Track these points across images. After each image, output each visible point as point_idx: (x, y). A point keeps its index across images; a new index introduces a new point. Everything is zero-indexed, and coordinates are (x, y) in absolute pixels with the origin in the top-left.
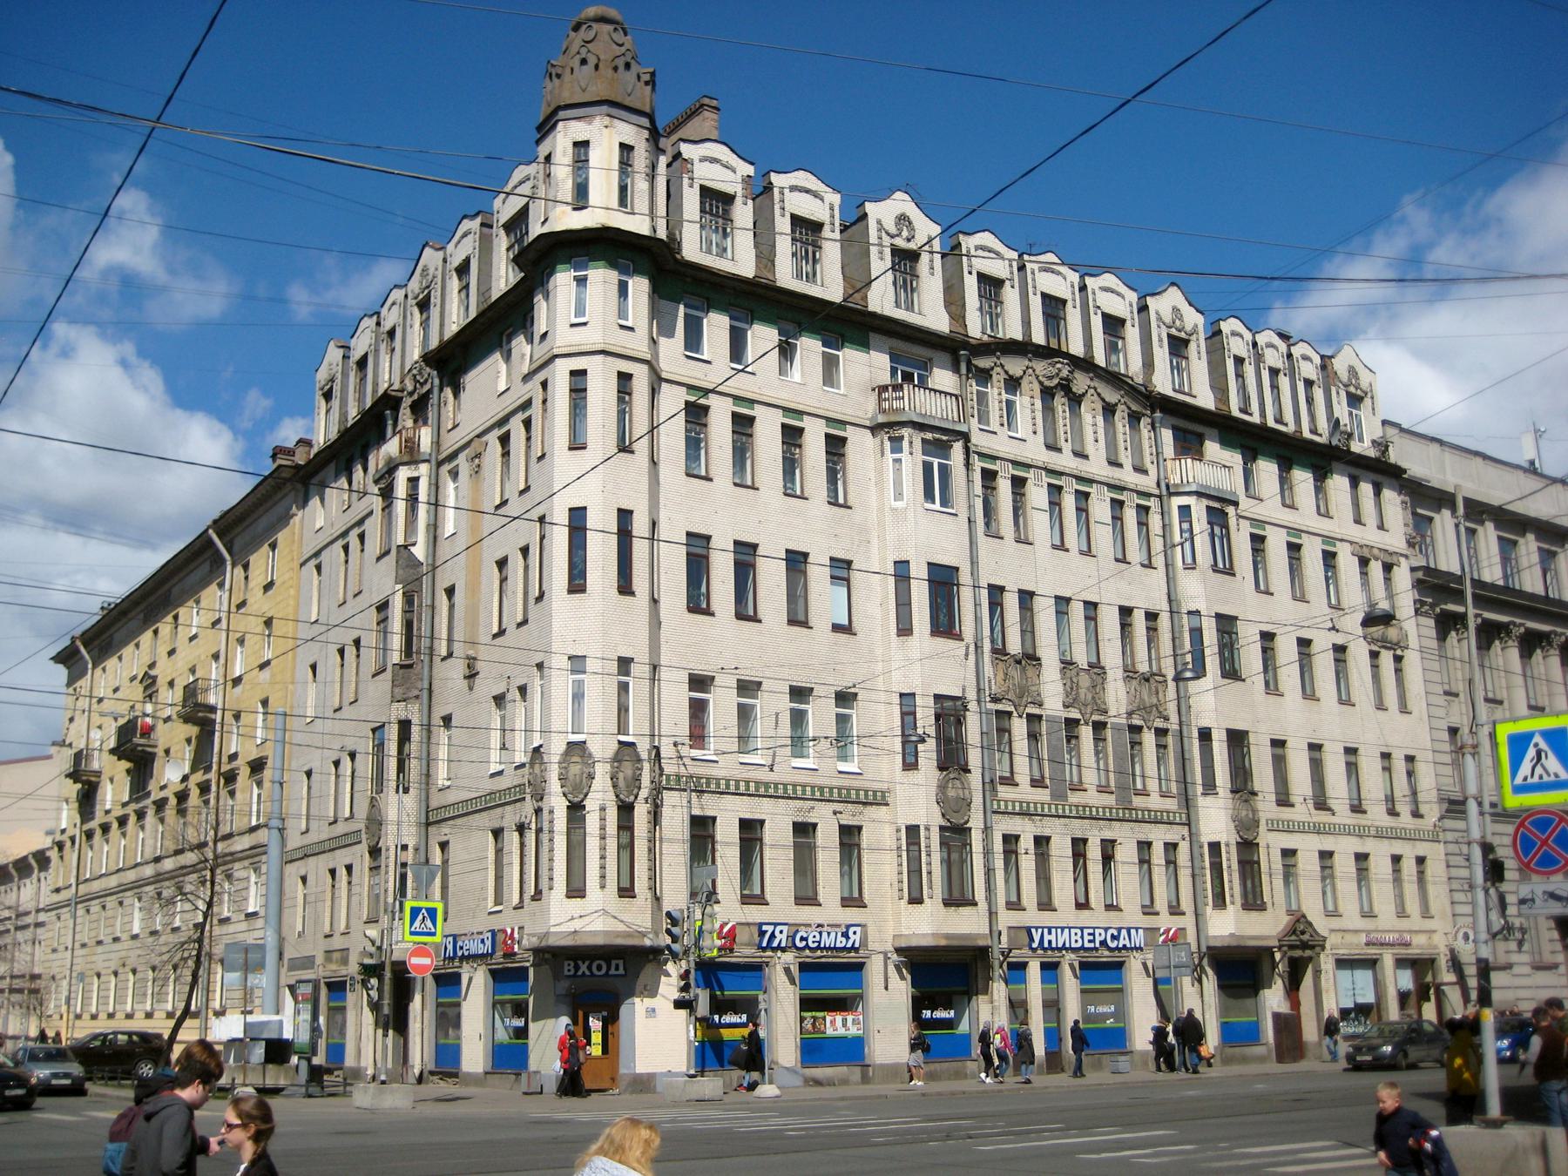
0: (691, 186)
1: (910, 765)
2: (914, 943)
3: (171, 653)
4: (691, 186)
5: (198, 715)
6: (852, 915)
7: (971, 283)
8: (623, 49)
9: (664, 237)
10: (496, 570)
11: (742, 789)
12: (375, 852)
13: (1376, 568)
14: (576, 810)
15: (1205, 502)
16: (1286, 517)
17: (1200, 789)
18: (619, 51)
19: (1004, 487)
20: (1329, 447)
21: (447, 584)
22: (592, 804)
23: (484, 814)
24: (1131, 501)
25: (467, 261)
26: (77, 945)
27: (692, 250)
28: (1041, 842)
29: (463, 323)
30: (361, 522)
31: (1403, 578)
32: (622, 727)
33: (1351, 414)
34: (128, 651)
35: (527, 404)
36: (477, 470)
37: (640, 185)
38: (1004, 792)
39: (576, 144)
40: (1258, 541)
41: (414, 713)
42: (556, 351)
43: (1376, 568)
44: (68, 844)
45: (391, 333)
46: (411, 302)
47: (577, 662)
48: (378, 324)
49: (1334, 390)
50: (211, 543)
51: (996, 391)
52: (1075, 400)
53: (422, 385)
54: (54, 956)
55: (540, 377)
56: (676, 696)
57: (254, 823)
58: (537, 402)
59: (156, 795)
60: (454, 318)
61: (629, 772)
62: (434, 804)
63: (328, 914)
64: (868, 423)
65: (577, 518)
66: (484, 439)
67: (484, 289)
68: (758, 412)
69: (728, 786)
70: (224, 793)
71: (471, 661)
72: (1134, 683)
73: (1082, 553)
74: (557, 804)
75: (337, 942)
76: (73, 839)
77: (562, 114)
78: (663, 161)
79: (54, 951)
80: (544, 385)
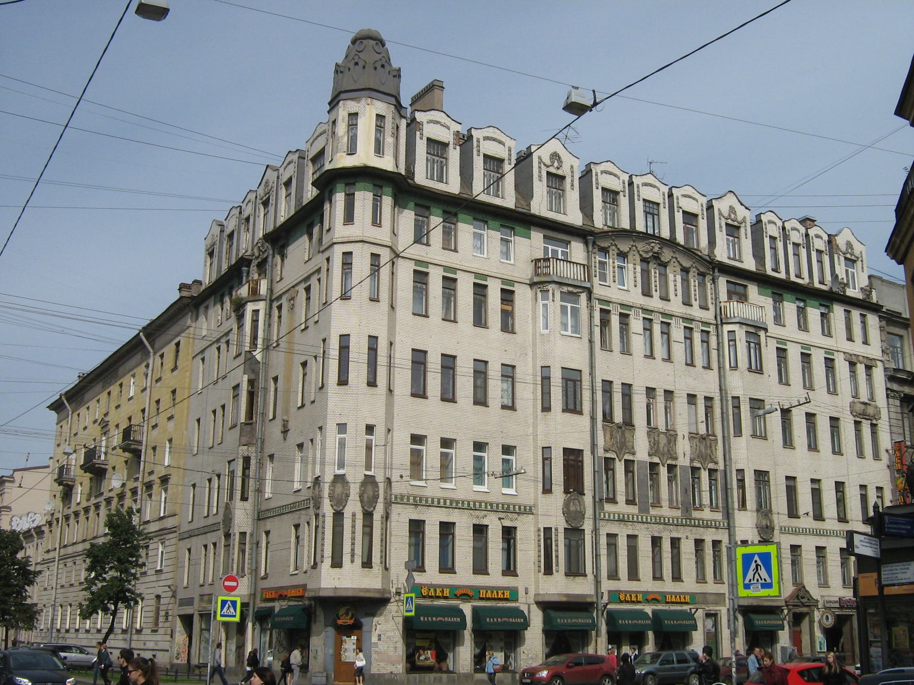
0: (421, 139)
2: (547, 599)
3: (118, 407)
5: (131, 447)
6: (508, 581)
7: (597, 195)
8: (381, 56)
11: (442, 504)
12: (228, 536)
13: (861, 369)
14: (338, 516)
15: (745, 328)
16: (802, 337)
17: (736, 506)
18: (378, 57)
19: (615, 320)
20: (831, 291)
22: (347, 513)
23: (290, 515)
24: (697, 328)
25: (290, 180)
26: (59, 586)
27: (421, 178)
28: (632, 538)
29: (287, 217)
30: (227, 334)
31: (879, 374)
32: (368, 467)
33: (847, 271)
34: (92, 404)
35: (318, 271)
36: (292, 308)
37: (389, 140)
38: (608, 507)
39: (350, 115)
40: (782, 353)
41: (252, 452)
42: (335, 240)
43: (861, 369)
44: (55, 522)
45: (248, 219)
46: (259, 201)
47: (342, 428)
48: (240, 213)
49: (836, 256)
50: (141, 342)
51: (611, 261)
52: (664, 265)
53: (263, 253)
54: (45, 593)
56: (402, 448)
57: (162, 515)
58: (324, 270)
59: (107, 495)
60: (283, 214)
61: (371, 494)
62: (263, 508)
63: (202, 570)
64: (528, 282)
66: (297, 288)
67: (299, 198)
70: (145, 496)
71: (285, 424)
72: (695, 440)
73: (663, 360)
74: (327, 509)
75: (207, 590)
77: (343, 96)
78: (403, 123)
79: (45, 589)
80: (328, 259)
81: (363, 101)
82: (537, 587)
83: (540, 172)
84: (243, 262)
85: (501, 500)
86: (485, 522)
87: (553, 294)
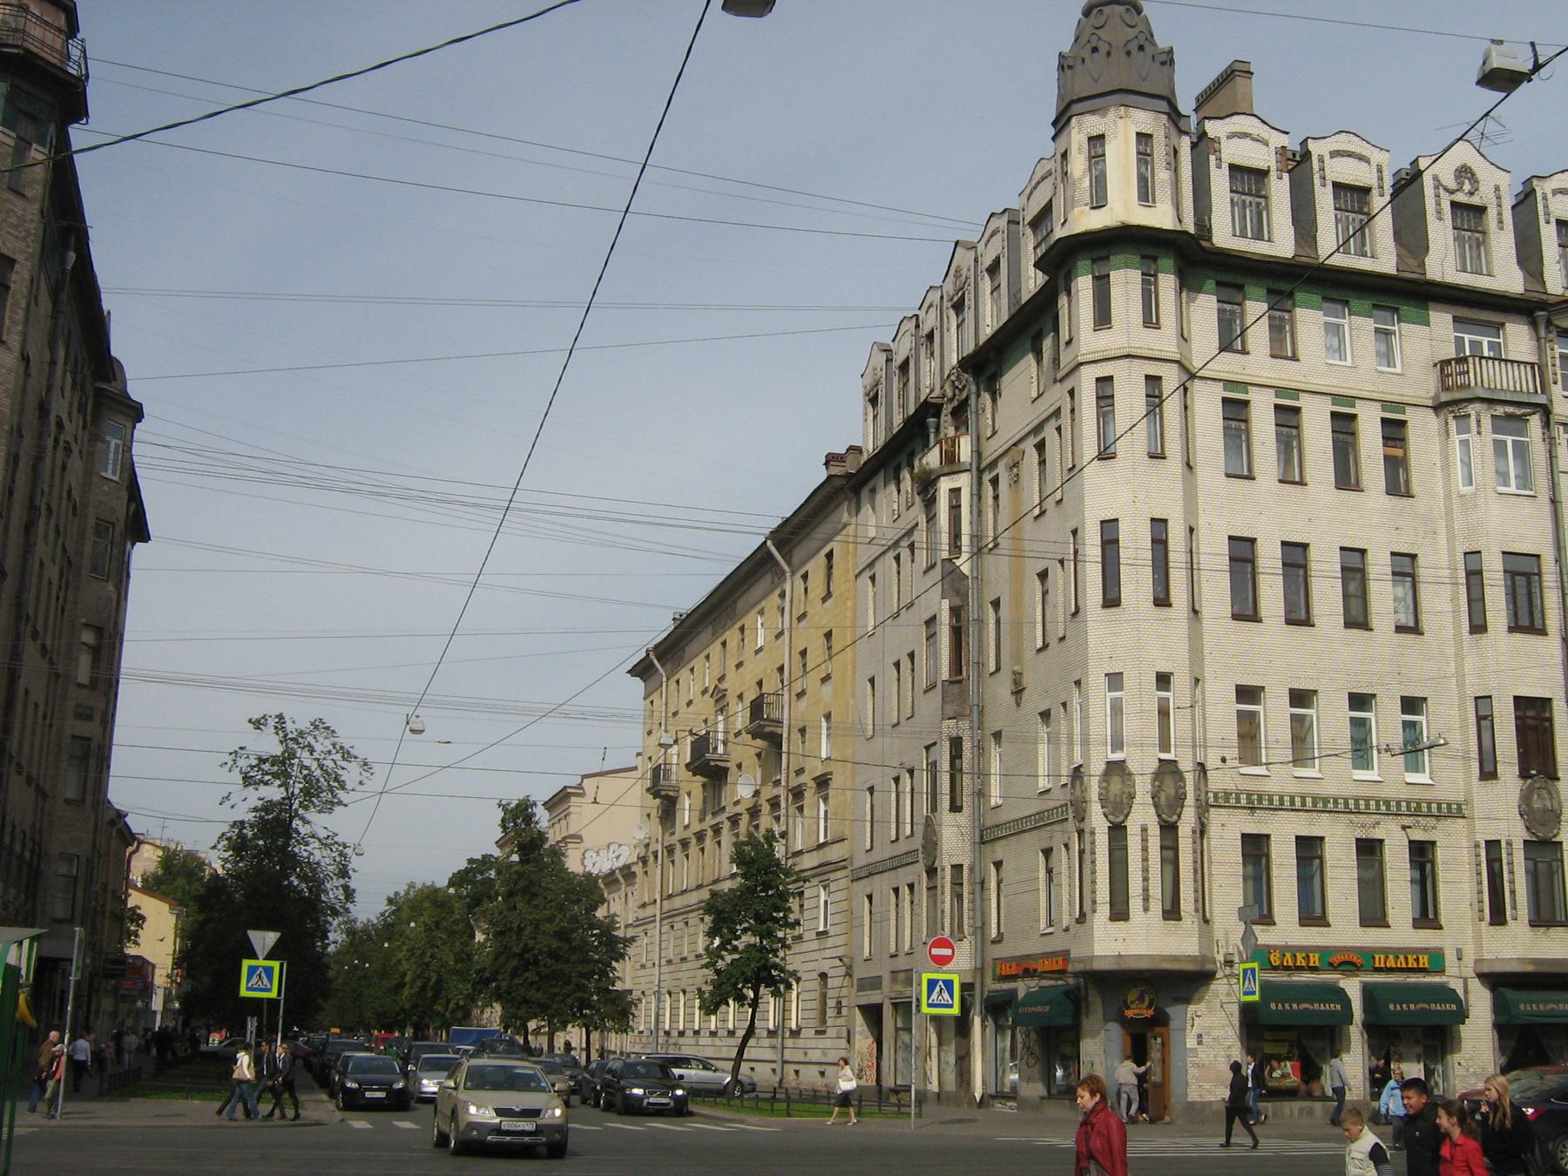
1: (1488, 773)
2: (1498, 968)
3: (739, 665)
4: (1219, 167)
8: (1136, 30)
9: (1192, 231)
10: (1038, 582)
11: (1298, 804)
12: (932, 872)
14: (1117, 831)
18: (1131, 33)
21: (993, 598)
26: (663, 962)
29: (996, 326)
30: (910, 532)
32: (1164, 745)
34: (699, 662)
35: (1057, 413)
36: (1016, 480)
37: (1162, 175)
41: (964, 728)
42: (1081, 359)
45: (930, 336)
46: (947, 304)
48: (917, 326)
53: (961, 390)
54: (642, 972)
55: (1068, 384)
57: (822, 840)
58: (1066, 411)
59: (731, 810)
60: (988, 321)
61: (1172, 792)
64: (1430, 403)
65: (1109, 527)
66: (1021, 446)
67: (1014, 290)
68: (1304, 402)
69: (1282, 802)
70: (792, 809)
74: (1098, 821)
75: (902, 963)
76: (655, 854)
77: (1076, 108)
78: (1185, 144)
79: (643, 967)
80: (1071, 393)
81: (1112, 114)
82: (1479, 946)
83: (1438, 204)
84: (929, 409)
85: (1405, 794)
86: (1377, 834)
87: (1478, 421)
